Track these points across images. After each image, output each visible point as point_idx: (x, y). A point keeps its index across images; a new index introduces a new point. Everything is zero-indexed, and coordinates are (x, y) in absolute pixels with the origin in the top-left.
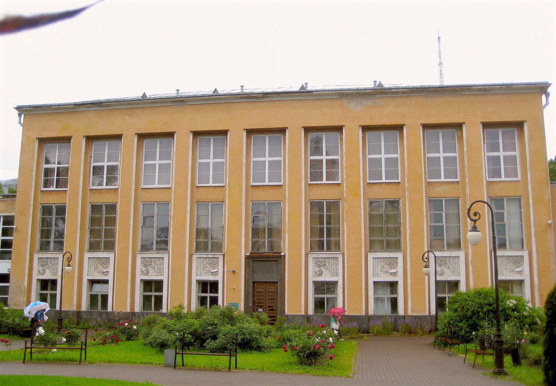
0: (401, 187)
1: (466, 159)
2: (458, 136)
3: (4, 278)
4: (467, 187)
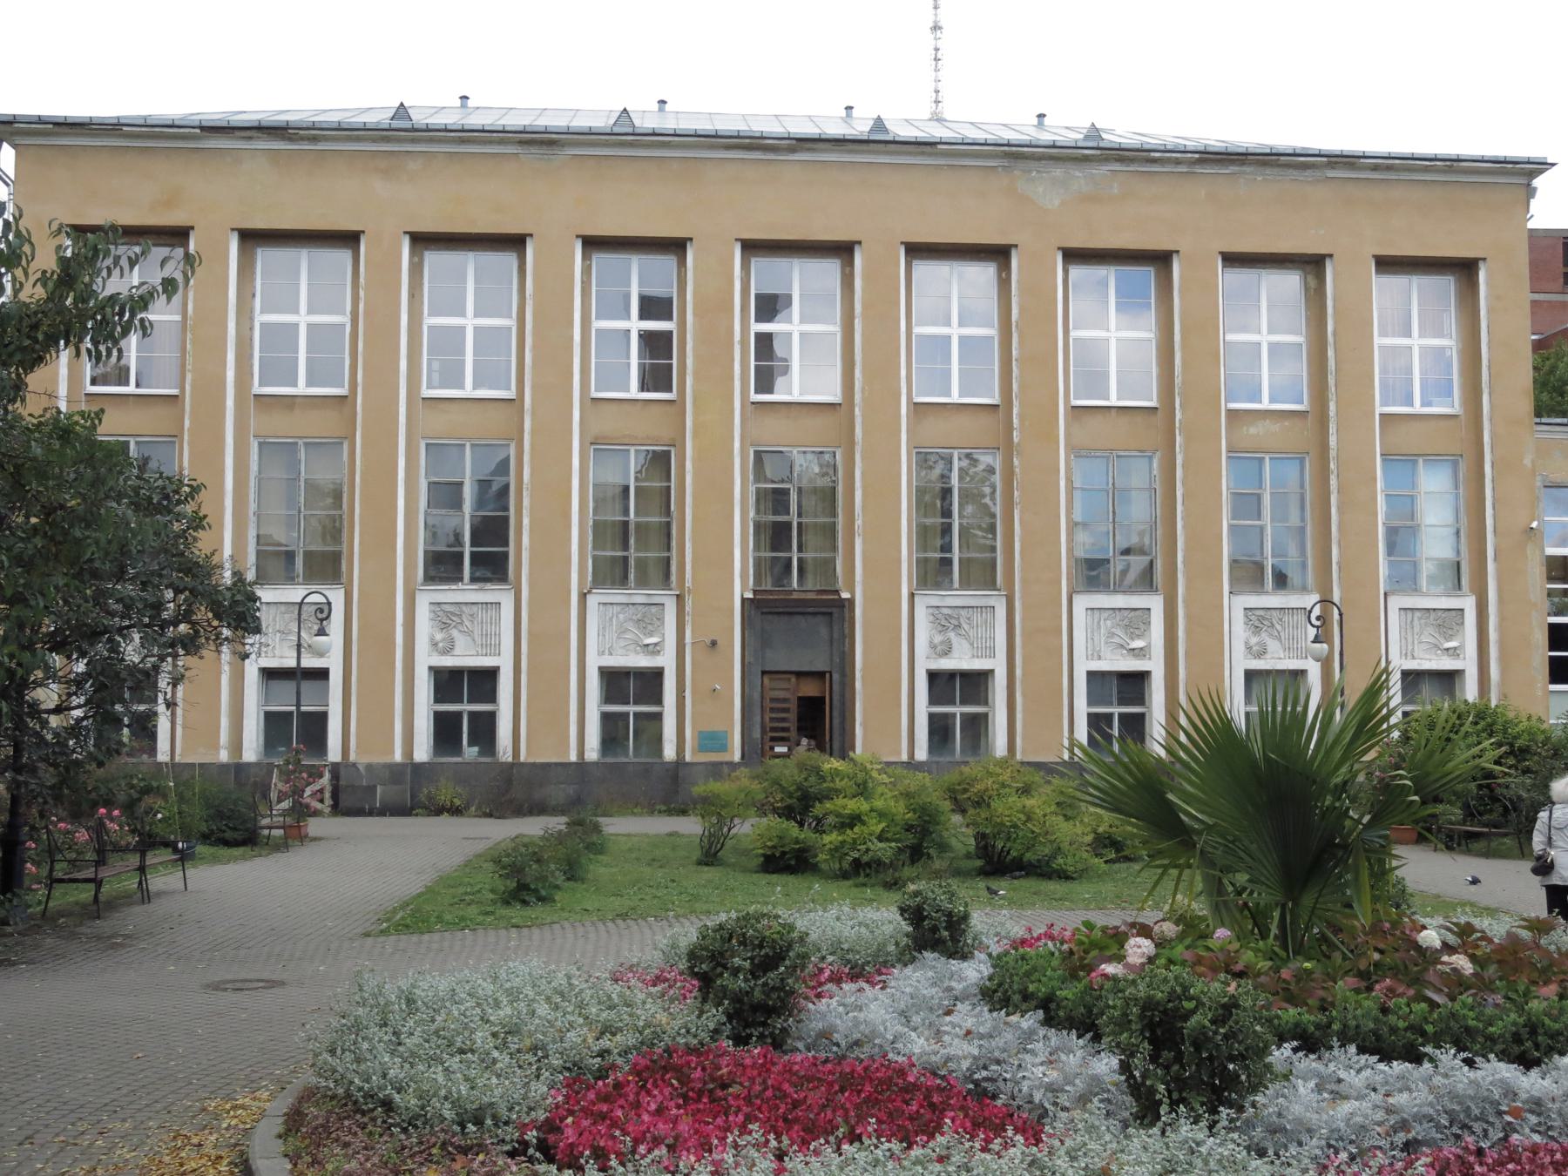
1: (1331, 353)
3: (1561, 672)
4: (1332, 429)
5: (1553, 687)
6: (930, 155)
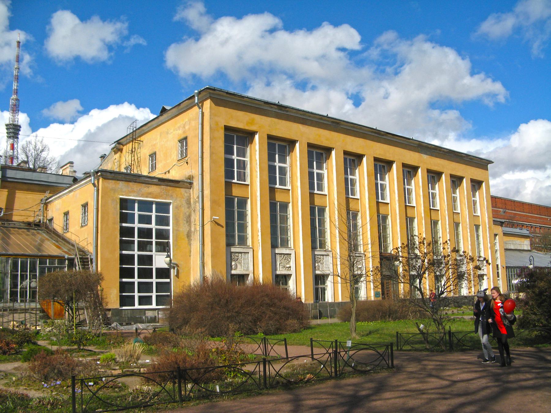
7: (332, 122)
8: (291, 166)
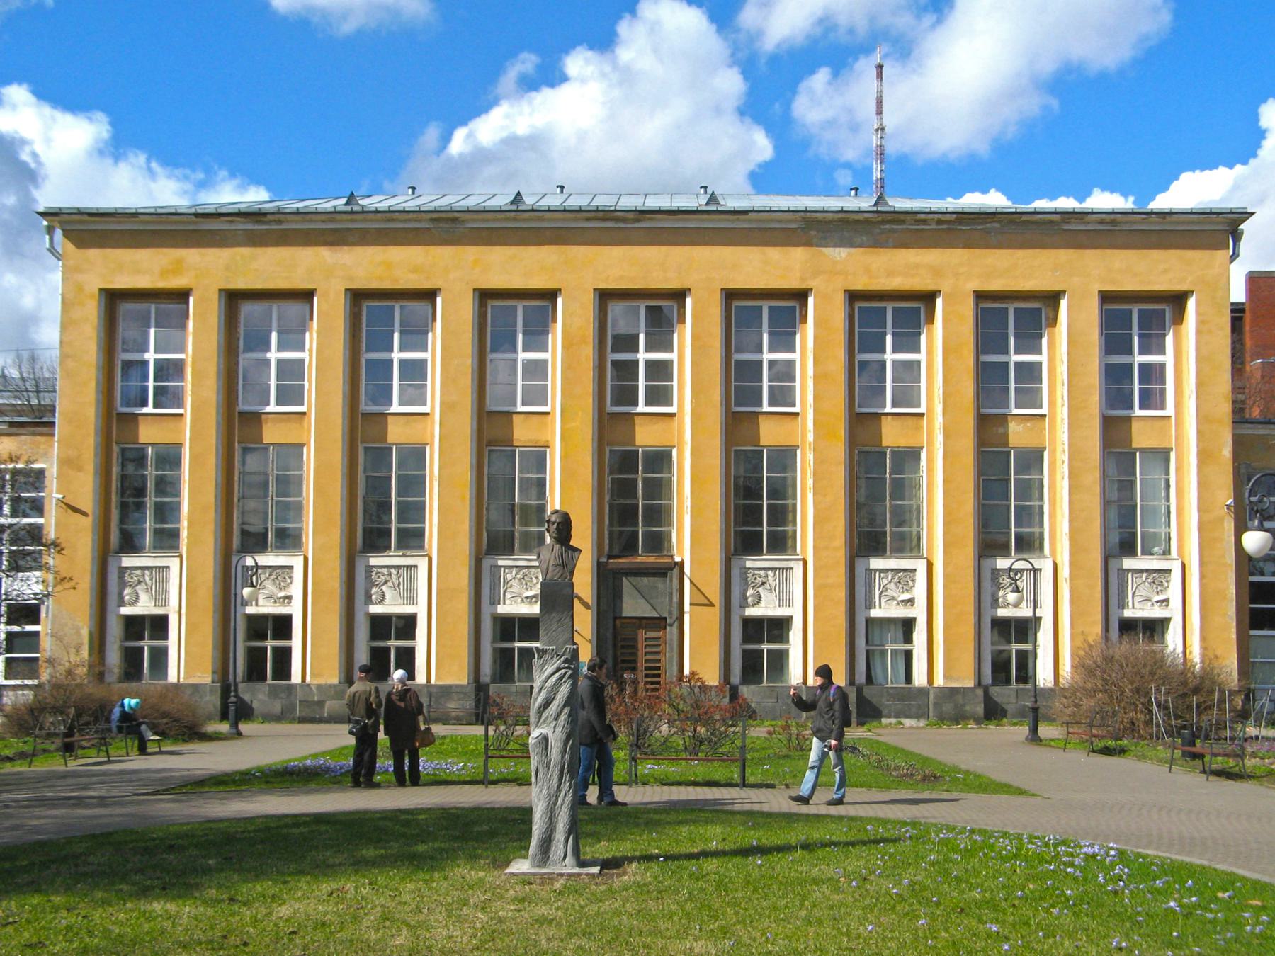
0: (550, 417)
2: (1047, 319)
5: (1253, 633)
6: (744, 220)
7: (432, 220)
8: (1051, 359)
